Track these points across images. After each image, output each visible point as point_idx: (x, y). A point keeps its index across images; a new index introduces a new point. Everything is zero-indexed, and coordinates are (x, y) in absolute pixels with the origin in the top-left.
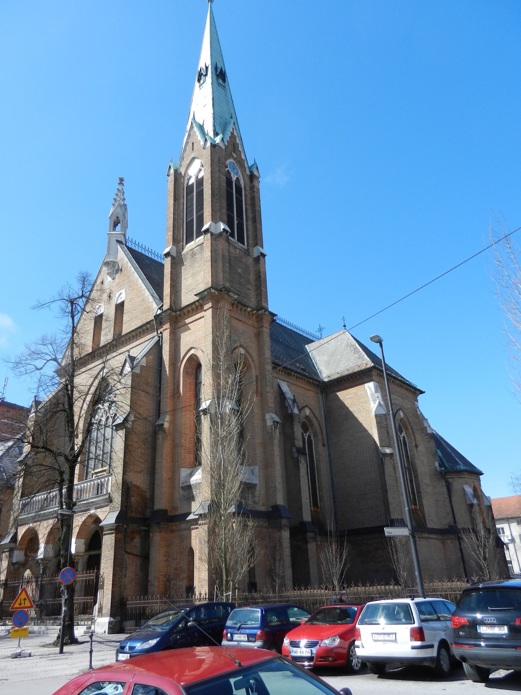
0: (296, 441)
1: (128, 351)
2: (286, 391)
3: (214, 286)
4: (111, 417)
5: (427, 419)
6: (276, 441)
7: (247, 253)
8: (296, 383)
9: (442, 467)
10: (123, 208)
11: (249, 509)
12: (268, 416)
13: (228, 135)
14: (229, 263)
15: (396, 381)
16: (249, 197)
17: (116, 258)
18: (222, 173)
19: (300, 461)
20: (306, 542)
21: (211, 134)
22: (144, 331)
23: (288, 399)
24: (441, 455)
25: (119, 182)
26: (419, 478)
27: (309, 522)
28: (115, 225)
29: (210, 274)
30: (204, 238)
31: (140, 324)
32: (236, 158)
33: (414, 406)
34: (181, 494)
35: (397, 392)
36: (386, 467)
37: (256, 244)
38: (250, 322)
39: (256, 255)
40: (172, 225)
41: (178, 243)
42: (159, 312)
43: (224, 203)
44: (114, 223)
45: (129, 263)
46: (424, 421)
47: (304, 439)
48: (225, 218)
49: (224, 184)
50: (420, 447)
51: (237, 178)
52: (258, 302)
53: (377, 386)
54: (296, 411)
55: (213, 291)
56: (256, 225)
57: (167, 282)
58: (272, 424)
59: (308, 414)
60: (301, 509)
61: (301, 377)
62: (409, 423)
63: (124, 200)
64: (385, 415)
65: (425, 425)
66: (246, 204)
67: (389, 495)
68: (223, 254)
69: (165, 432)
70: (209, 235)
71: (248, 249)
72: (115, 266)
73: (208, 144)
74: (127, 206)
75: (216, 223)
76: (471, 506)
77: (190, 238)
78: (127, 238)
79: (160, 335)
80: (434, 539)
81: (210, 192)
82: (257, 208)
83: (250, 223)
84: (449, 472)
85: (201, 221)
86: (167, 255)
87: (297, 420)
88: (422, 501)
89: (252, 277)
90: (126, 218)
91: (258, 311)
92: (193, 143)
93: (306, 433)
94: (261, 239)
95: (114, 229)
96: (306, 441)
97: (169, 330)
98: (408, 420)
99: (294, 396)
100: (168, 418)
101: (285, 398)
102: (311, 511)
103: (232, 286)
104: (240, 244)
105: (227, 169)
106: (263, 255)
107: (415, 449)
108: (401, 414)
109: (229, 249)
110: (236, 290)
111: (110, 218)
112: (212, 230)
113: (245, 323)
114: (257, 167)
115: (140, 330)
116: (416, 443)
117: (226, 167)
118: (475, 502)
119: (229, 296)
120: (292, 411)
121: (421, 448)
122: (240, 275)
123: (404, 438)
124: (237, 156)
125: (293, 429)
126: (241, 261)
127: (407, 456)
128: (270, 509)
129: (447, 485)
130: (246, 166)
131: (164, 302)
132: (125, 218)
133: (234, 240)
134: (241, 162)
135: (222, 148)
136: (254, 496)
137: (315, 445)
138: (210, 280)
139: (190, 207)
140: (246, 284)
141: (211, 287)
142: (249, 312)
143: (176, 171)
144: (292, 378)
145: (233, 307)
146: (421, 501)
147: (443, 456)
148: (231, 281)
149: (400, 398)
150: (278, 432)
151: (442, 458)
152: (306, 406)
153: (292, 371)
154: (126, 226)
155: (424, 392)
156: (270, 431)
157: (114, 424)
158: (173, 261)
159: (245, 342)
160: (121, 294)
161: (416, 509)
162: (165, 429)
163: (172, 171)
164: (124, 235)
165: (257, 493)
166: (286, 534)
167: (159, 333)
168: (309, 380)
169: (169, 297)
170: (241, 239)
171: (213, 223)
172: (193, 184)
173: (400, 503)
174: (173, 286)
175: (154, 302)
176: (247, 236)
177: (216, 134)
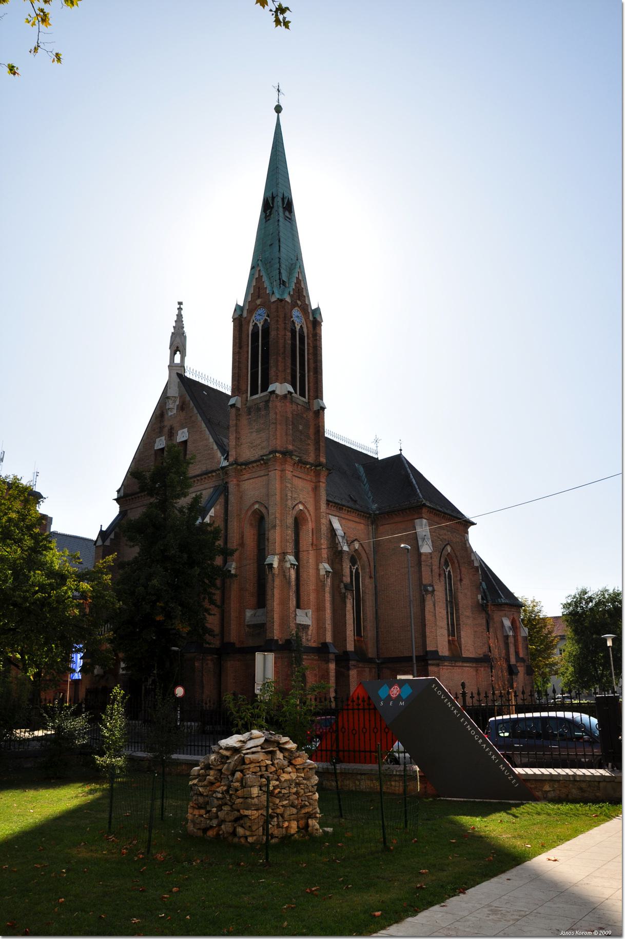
0: (344, 577)
2: (337, 528)
6: (328, 589)
7: (308, 405)
8: (347, 517)
12: (321, 566)
20: (348, 669)
24: (485, 587)
25: (182, 306)
27: (351, 652)
34: (246, 631)
36: (427, 603)
38: (309, 478)
50: (464, 580)
51: (301, 326)
56: (317, 376)
58: (325, 573)
59: (357, 548)
61: (352, 510)
64: (430, 553)
66: (308, 353)
67: (427, 629)
71: (309, 402)
76: (507, 637)
80: (468, 667)
89: (312, 431)
96: (354, 575)
101: (336, 534)
102: (354, 640)
107: (459, 583)
108: (449, 549)
112: (278, 392)
118: (511, 633)
119: (292, 458)
121: (466, 581)
122: (301, 432)
123: (449, 571)
124: (302, 302)
125: (342, 566)
126: (303, 417)
127: (451, 590)
135: (288, 302)
136: (307, 634)
137: (362, 577)
146: (459, 633)
147: (487, 589)
149: (449, 533)
150: (329, 580)
151: (486, 590)
152: (356, 540)
153: (344, 506)
155: (476, 524)
156: (323, 580)
161: (453, 640)
165: (310, 632)
166: (332, 666)
168: (360, 513)
173: (437, 636)
176: (308, 368)
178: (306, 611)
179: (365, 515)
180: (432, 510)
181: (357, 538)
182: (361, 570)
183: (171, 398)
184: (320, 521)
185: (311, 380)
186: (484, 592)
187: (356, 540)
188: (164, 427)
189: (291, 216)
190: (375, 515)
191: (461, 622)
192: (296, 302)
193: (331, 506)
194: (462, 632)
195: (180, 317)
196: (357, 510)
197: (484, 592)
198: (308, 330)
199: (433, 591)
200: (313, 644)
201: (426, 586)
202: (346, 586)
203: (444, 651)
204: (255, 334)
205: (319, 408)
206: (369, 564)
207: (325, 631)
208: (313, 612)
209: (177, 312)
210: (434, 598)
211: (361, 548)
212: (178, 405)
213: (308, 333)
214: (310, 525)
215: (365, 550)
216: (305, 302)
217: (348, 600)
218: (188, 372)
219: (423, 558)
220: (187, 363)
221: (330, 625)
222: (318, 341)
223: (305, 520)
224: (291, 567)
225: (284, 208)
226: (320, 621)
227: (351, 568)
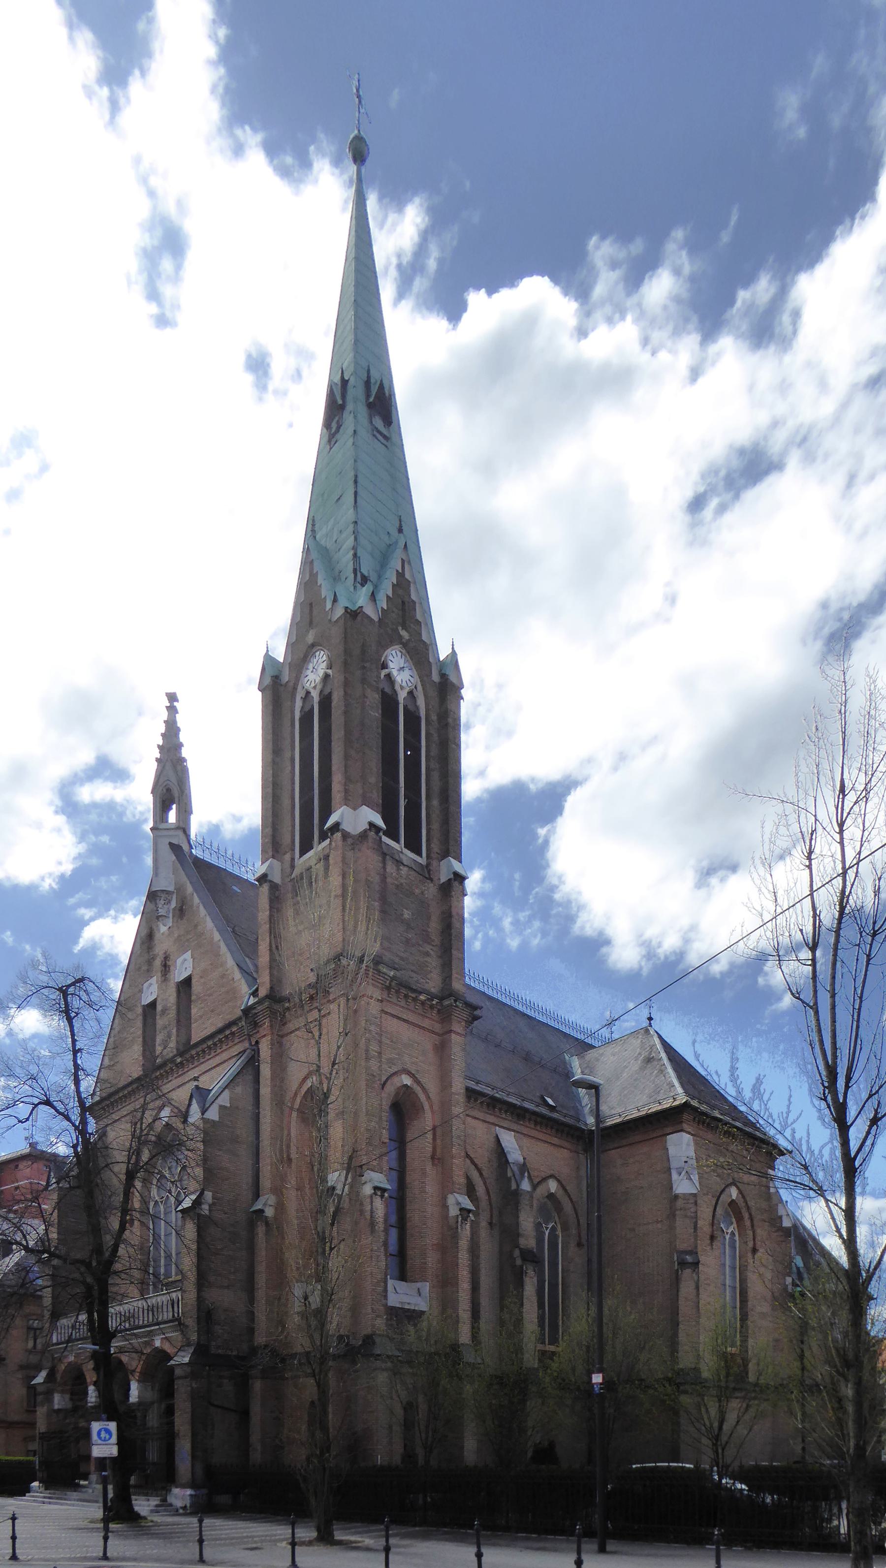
1: (196, 1079)
4: (162, 1202)
7: (426, 873)
12: (451, 1200)
19: (526, 1273)
23: (511, 1165)
26: (749, 1303)
32: (409, 640)
38: (426, 1023)
42: (252, 1001)
46: (780, 1206)
48: (376, 796)
49: (376, 714)
51: (411, 693)
54: (526, 1186)
64: (695, 1195)
65: (781, 1212)
68: (367, 880)
71: (428, 865)
83: (435, 802)
89: (434, 926)
91: (441, 999)
93: (547, 1223)
100: (272, 1199)
101: (507, 1161)
105: (384, 673)
107: (750, 1255)
110: (398, 956)
112: (345, 826)
116: (754, 1244)
120: (518, 1186)
124: (411, 636)
125: (518, 1217)
130: (431, 660)
135: (371, 620)
142: (423, 1003)
152: (552, 1176)
157: (180, 1208)
160: (151, 984)
170: (413, 845)
178: (419, 1285)
181: (552, 1172)
183: (159, 894)
187: (552, 1176)
188: (154, 959)
189: (389, 431)
195: (171, 731)
199: (696, 1264)
204: (307, 718)
205: (452, 876)
206: (578, 1221)
207: (458, 1322)
208: (432, 1287)
209: (165, 715)
210: (698, 1274)
212: (174, 909)
213: (427, 710)
214: (428, 1119)
215: (569, 1196)
216: (420, 634)
221: (469, 1313)
223: (417, 1109)
224: (375, 1194)
225: (370, 406)
226: (447, 1303)
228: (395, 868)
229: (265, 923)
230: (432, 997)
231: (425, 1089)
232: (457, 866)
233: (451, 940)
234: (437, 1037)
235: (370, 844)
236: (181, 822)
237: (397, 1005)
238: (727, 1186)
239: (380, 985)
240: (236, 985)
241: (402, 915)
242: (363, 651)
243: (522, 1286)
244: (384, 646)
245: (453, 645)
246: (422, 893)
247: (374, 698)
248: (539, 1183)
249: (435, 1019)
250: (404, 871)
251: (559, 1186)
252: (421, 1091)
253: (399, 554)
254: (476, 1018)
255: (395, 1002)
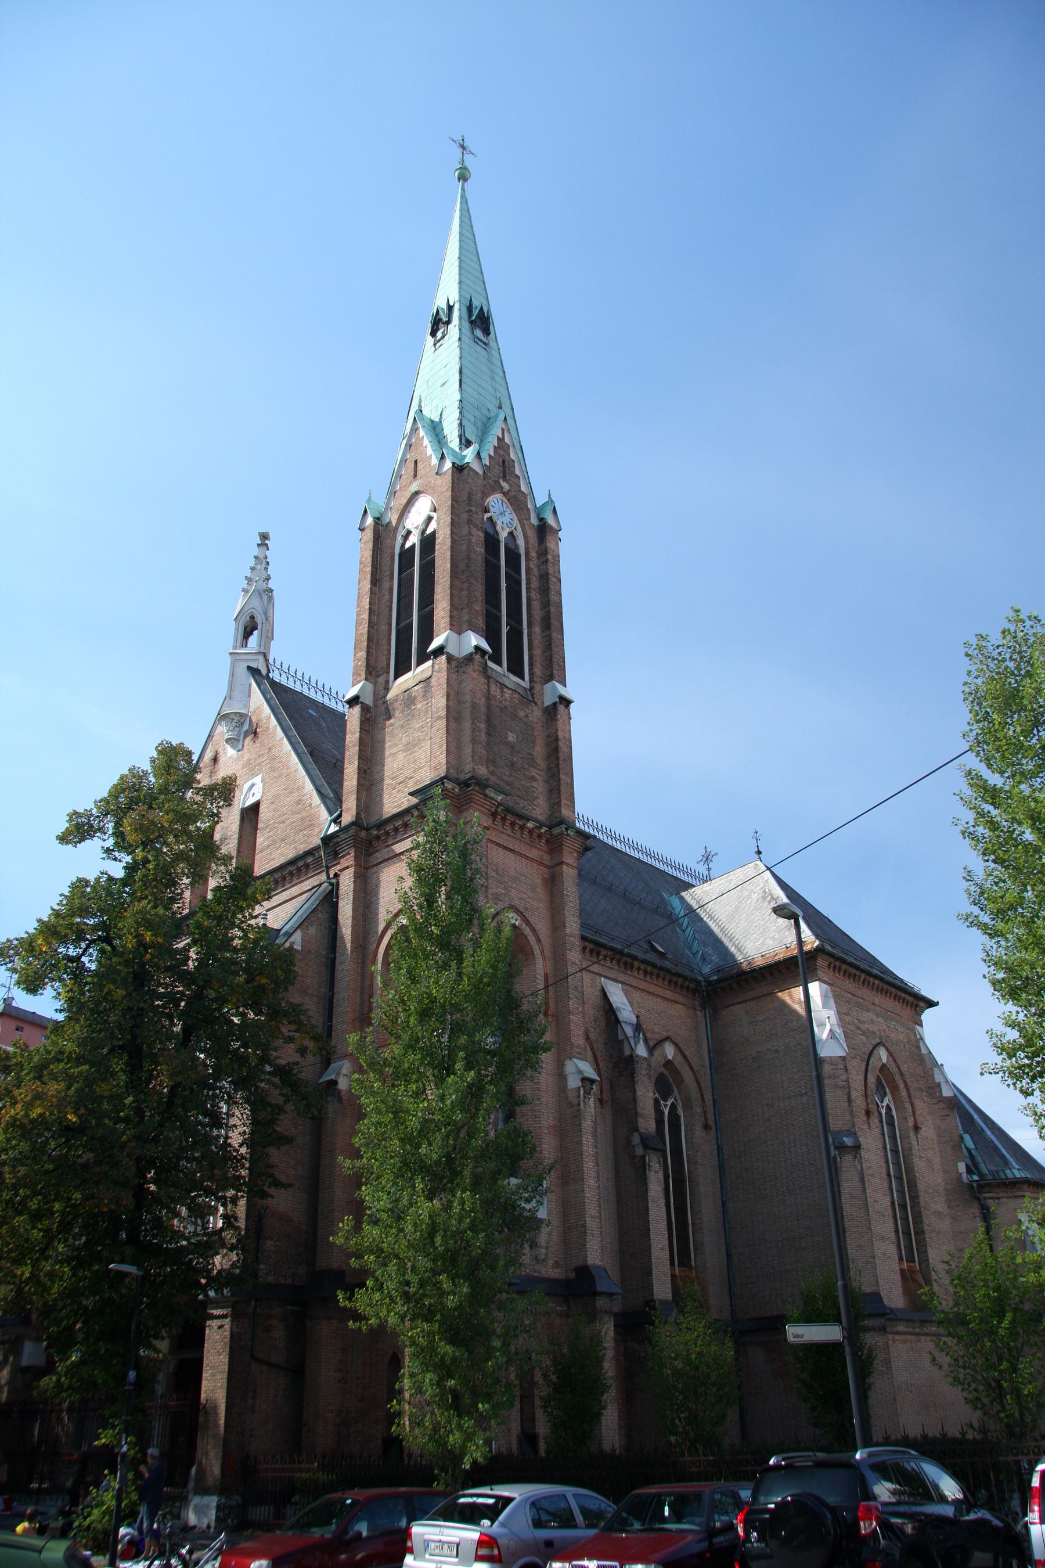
2: (620, 1006)
3: (453, 773)
5: (942, 1065)
7: (530, 697)
9: (973, 1173)
10: (265, 598)
11: (523, 1273)
12: (570, 1067)
13: (491, 442)
14: (488, 720)
15: (871, 979)
16: (536, 573)
17: (247, 705)
18: (476, 526)
19: (649, 1166)
21: (454, 443)
22: (299, 869)
23: (623, 1025)
24: (971, 1145)
26: (921, 1199)
28: (248, 632)
29: (444, 747)
30: (433, 666)
31: (291, 855)
32: (509, 491)
33: (913, 1037)
35: (874, 1004)
37: (550, 678)
38: (534, 853)
39: (549, 700)
40: (365, 637)
41: (378, 676)
42: (334, 828)
43: (479, 590)
44: (245, 628)
45: (272, 717)
47: (659, 1113)
48: (481, 622)
49: (480, 549)
51: (511, 534)
52: (552, 807)
53: (826, 992)
54: (641, 1051)
55: (449, 785)
56: (550, 634)
57: (351, 763)
59: (670, 1057)
60: (649, 1272)
61: (656, 971)
62: (902, 1074)
63: (268, 578)
64: (843, 1058)
65: (938, 1078)
66: (528, 589)
67: (848, 1239)
69: (340, 1099)
70: (444, 657)
71: (531, 688)
72: (242, 724)
73: (448, 465)
74: (274, 593)
75: (459, 633)
77: (403, 668)
78: (271, 661)
79: (334, 881)
81: (449, 565)
82: (553, 597)
83: (537, 629)
84: (989, 1185)
85: (427, 633)
86: (353, 702)
87: (644, 1072)
88: (926, 1251)
89: (539, 751)
90: (270, 619)
91: (551, 827)
92: (416, 462)
93: (665, 1100)
94: (560, 666)
95: (245, 644)
96: (666, 1119)
97: (352, 870)
98: (899, 1069)
99: (637, 1017)
101: (617, 1021)
102: (673, 1276)
103: (492, 773)
104: (512, 676)
105: (487, 515)
106: (566, 702)
107: (912, 1134)
108: (883, 1055)
109: (489, 691)
110: (503, 780)
111: (235, 619)
112: (449, 649)
113: (521, 855)
114: (554, 508)
115: (292, 868)
117: (487, 510)
119: (486, 796)
121: (928, 1131)
122: (512, 747)
124: (511, 486)
125: (635, 1092)
126: (516, 716)
127: (895, 1151)
128: (572, 1275)
129: (984, 1214)
131: (344, 806)
132: (267, 619)
133: (499, 670)
134: (518, 501)
135: (476, 473)
138: (442, 759)
139: (405, 596)
140: (526, 766)
141: (445, 777)
142: (531, 832)
143: (377, 520)
144: (635, 973)
145: (494, 820)
148: (490, 761)
149: (880, 1019)
151: (973, 1152)
152: (667, 1038)
154: (270, 635)
155: (936, 1004)
156: (575, 1101)
158: (366, 714)
159: (521, 899)
160: (253, 785)
161: (912, 1271)
162: (340, 1091)
163: (370, 521)
164: (265, 656)
165: (542, 1239)
166: (608, 1330)
167: (332, 876)
168: (674, 979)
169: (354, 796)
170: (516, 668)
171: (454, 635)
172: (413, 546)
174: (365, 772)
175: (323, 807)
177: (466, 443)
179: (686, 983)
180: (838, 964)
182: (684, 1112)
184: (564, 955)
185: (536, 642)
186: (972, 1157)
187: (667, 1038)
190: (709, 983)
191: (926, 1227)
192: (497, 483)
193: (605, 957)
194: (929, 1250)
196: (668, 971)
197: (972, 1157)
198: (527, 543)
199: (857, 1147)
200: (550, 1271)
201: (839, 1133)
202: (645, 1141)
203: (894, 1297)
211: (680, 1058)
213: (527, 549)
217: (652, 1173)
218: (277, 672)
219: (827, 1069)
220: (277, 652)
222: (550, 565)
225: (471, 322)
227: (656, 1102)
228: (499, 691)
229: (354, 745)
230: (541, 825)
231: (535, 930)
232: (562, 690)
233: (558, 764)
234: (546, 870)
235: (476, 667)
236: (262, 647)
237: (502, 832)
238: (875, 1047)
239: (486, 811)
240: (313, 811)
241: (506, 738)
242: (470, 499)
243: (646, 1184)
244: (486, 495)
245: (549, 495)
246: (526, 716)
247: (479, 536)
248: (655, 1047)
249: (544, 849)
250: (508, 694)
251: (677, 1051)
252: (532, 935)
253: (499, 424)
254: (587, 849)
255: (501, 829)
